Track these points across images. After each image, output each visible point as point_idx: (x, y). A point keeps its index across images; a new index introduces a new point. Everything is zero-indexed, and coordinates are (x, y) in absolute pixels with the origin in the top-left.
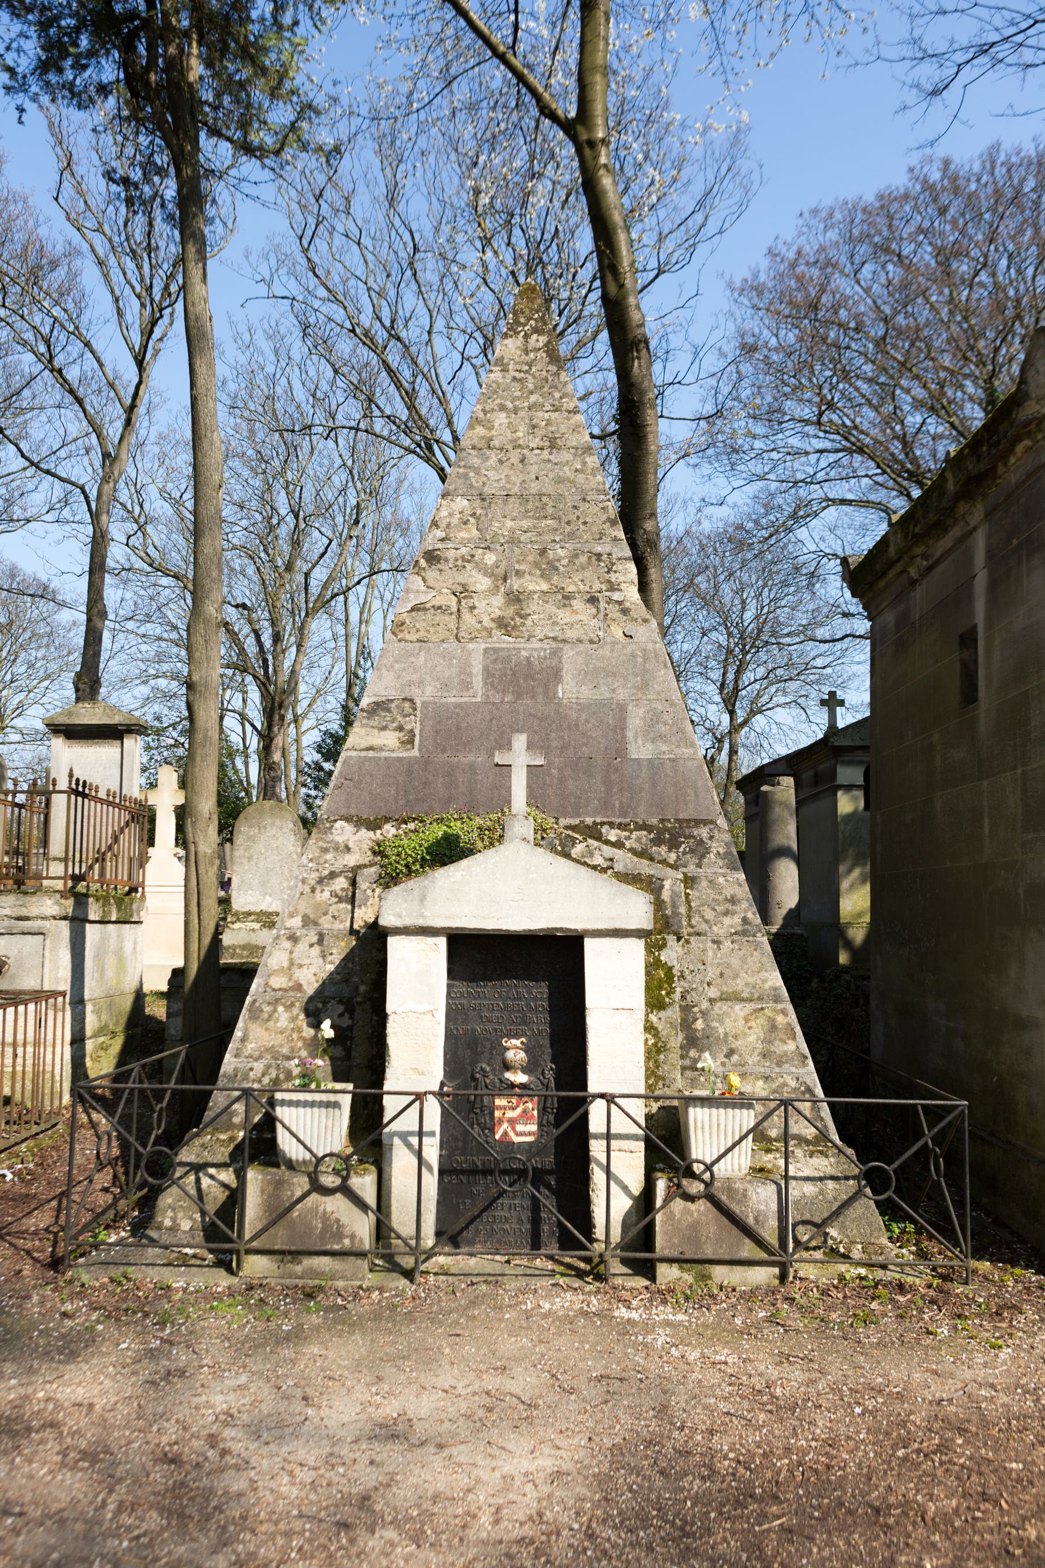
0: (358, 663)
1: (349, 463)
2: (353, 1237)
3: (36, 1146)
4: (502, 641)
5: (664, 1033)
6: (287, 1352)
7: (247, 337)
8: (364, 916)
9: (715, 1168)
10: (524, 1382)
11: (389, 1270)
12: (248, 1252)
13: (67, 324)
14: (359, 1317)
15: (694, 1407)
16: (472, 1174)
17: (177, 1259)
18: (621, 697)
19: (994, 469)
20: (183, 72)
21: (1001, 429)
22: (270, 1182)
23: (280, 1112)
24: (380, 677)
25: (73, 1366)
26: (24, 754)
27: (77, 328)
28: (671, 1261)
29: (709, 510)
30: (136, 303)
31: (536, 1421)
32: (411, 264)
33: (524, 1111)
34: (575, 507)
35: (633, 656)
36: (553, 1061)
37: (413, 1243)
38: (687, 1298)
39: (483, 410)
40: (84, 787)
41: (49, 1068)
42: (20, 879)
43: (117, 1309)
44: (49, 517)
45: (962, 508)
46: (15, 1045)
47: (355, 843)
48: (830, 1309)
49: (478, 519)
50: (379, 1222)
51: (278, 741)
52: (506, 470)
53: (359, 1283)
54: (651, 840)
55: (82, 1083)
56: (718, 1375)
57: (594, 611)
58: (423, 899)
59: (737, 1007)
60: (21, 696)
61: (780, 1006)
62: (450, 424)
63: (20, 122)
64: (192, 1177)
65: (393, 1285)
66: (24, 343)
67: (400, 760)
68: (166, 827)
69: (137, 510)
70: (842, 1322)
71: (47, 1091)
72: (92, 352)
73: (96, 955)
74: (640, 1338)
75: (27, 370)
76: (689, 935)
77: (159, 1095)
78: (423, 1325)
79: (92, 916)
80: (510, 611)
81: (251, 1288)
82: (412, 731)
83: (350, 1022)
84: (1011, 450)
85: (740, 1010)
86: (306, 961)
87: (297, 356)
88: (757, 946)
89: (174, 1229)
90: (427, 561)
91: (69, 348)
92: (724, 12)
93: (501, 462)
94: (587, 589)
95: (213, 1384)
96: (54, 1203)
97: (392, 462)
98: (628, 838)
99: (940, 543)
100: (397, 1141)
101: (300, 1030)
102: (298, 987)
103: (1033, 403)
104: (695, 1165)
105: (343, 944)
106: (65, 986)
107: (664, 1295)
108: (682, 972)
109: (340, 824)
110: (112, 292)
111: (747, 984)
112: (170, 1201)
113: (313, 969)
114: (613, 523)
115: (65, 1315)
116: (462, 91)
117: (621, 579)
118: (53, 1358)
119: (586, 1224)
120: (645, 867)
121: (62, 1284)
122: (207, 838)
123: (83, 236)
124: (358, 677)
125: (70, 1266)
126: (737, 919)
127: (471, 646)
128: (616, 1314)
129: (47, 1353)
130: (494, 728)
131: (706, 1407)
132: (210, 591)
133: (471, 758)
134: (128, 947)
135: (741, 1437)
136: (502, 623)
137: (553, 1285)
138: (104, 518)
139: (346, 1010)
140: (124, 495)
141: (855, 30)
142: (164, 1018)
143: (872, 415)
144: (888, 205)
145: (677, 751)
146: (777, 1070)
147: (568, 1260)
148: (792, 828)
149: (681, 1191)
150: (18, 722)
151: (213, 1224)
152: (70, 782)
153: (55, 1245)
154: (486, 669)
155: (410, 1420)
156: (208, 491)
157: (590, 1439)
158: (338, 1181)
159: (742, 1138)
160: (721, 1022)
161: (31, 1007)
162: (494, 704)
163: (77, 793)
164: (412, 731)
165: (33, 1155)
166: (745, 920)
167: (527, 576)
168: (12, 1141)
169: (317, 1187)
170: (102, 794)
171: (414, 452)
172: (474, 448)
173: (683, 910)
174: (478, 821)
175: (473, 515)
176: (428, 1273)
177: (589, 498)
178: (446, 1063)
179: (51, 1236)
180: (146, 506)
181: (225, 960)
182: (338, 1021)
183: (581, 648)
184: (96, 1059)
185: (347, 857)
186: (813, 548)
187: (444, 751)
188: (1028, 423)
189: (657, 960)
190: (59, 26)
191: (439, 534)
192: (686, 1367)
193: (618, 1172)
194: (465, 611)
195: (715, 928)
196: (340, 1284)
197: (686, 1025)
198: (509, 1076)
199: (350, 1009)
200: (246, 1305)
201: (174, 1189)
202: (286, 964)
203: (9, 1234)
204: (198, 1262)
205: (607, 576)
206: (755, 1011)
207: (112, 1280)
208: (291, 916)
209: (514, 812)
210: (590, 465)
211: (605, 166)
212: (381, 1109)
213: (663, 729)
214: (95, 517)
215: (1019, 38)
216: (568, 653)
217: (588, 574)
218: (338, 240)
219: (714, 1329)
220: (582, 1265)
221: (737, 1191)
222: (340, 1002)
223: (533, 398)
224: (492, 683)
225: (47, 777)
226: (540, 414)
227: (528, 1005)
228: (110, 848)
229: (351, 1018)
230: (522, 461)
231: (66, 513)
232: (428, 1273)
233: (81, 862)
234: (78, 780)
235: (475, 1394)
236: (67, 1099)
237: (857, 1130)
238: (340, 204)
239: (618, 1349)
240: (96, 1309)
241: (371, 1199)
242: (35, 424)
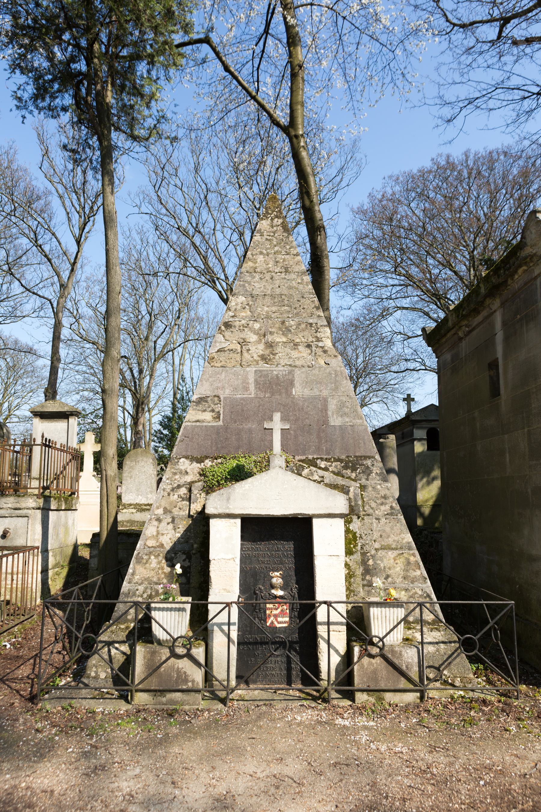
0: (179, 383)
2: (193, 681)
3: (23, 628)
4: (266, 367)
5: (353, 567)
6: (161, 752)
7: (128, 233)
9: (385, 640)
10: (293, 768)
11: (213, 699)
12: (137, 691)
13: (44, 225)
14: (199, 728)
15: (391, 783)
16: (254, 644)
17: (98, 695)
18: (325, 394)
19: (506, 281)
20: (104, 97)
21: (511, 262)
23: (154, 614)
25: (42, 765)
26: (19, 427)
27: (49, 227)
28: (362, 691)
29: (343, 312)
30: (77, 216)
31: (304, 794)
32: (206, 197)
33: (282, 610)
34: (298, 301)
35: (330, 374)
36: (297, 583)
37: (225, 683)
38: (373, 712)
39: (252, 254)
40: (49, 442)
41: (30, 586)
42: (18, 489)
43: (66, 726)
44: (35, 314)
45: (488, 301)
46: (12, 574)
47: (189, 470)
48: (450, 716)
49: (250, 306)
50: (206, 673)
51: (141, 420)
52: (263, 283)
53: (197, 707)
54: (343, 467)
55: (48, 600)
56: (399, 761)
57: (309, 351)
58: (228, 499)
59: (390, 553)
60: (19, 400)
61: (411, 552)
62: (224, 271)
63: (23, 122)
64: (106, 649)
65: (215, 708)
67: (213, 427)
68: (89, 462)
69: (75, 312)
70: (458, 724)
71: (29, 597)
72: (56, 238)
73: (54, 527)
74: (353, 737)
75: (25, 247)
76: (364, 515)
77: (88, 604)
78: (234, 732)
79: (52, 508)
80: (267, 352)
81: (139, 711)
82: (219, 412)
83: (189, 564)
84: (516, 272)
85: (391, 554)
86: (166, 532)
87: (151, 242)
88: (399, 521)
89: (96, 677)
90: (225, 327)
91: (45, 236)
92: (355, 81)
93: (261, 279)
94: (306, 340)
95: (121, 775)
96: (32, 661)
97: (195, 290)
98: (331, 466)
99: (476, 319)
100: (215, 628)
101: (163, 568)
102: (162, 546)
103: (529, 248)
104: (374, 639)
105: (185, 522)
106: (38, 544)
107: (361, 710)
108: (361, 535)
109: (182, 460)
110: (66, 210)
111: (394, 541)
112: (94, 662)
113: (169, 536)
114: (318, 308)
115: (37, 730)
116: (231, 120)
117: (323, 336)
118: (31, 759)
119: (316, 671)
120: (340, 481)
121: (35, 711)
122: (111, 468)
124: (179, 390)
125: (40, 700)
126: (388, 507)
127: (248, 369)
128: (337, 722)
129: (27, 756)
130: (261, 410)
131: (398, 782)
132: (114, 344)
133: (249, 425)
134: (70, 522)
135: (421, 802)
136: (263, 358)
137: (301, 705)
138: (60, 314)
139: (187, 557)
140: (69, 305)
141: (414, 91)
142: (88, 557)
143: (417, 269)
144: (423, 174)
145: (354, 421)
146: (412, 585)
147: (307, 691)
148: (395, 459)
149: (367, 653)
150: (17, 413)
151: (117, 675)
152: (42, 440)
153: (32, 687)
154: (256, 381)
155: (233, 796)
156: (114, 295)
157: (337, 806)
158: (185, 651)
159: (398, 624)
161: (21, 555)
162: (260, 398)
163: (46, 445)
164: (219, 412)
165: (21, 633)
166: (392, 507)
167: (275, 334)
168: (10, 626)
169: (174, 655)
170: (58, 446)
171: (207, 284)
172: (247, 272)
173: (360, 502)
174: (254, 458)
175: (248, 304)
176: (234, 700)
177: (305, 296)
178: (241, 585)
179: (30, 681)
180: (80, 311)
181: (120, 528)
183: (304, 369)
184: (54, 580)
185: (186, 477)
186: (390, 329)
187: (235, 422)
188: (526, 258)
190: (44, 80)
191: (231, 314)
192: (381, 756)
194: (244, 352)
195: (377, 512)
196: (187, 707)
197: (364, 562)
198: (274, 591)
199: (189, 557)
200: (137, 722)
201: (96, 656)
202: (155, 533)
203: (7, 680)
204: (110, 696)
205: (315, 334)
206: (399, 554)
208: (158, 508)
209: (275, 452)
210: (305, 280)
211: (303, 146)
212: (207, 611)
213: (346, 410)
214: (56, 314)
215: (489, 95)
216: (297, 372)
217: (306, 333)
218: (172, 188)
219: (391, 731)
220: (315, 693)
221: (396, 652)
222: (184, 553)
223: (276, 249)
224: (259, 388)
225: (31, 439)
226: (280, 256)
227: (283, 554)
228: (62, 472)
229: (189, 562)
230: (272, 278)
231: (42, 313)
232: (234, 700)
233: (47, 480)
234: (46, 439)
235: (268, 777)
236: (39, 601)
237: (453, 617)
238: (172, 171)
239: (341, 744)
240: (55, 726)
241: (202, 660)
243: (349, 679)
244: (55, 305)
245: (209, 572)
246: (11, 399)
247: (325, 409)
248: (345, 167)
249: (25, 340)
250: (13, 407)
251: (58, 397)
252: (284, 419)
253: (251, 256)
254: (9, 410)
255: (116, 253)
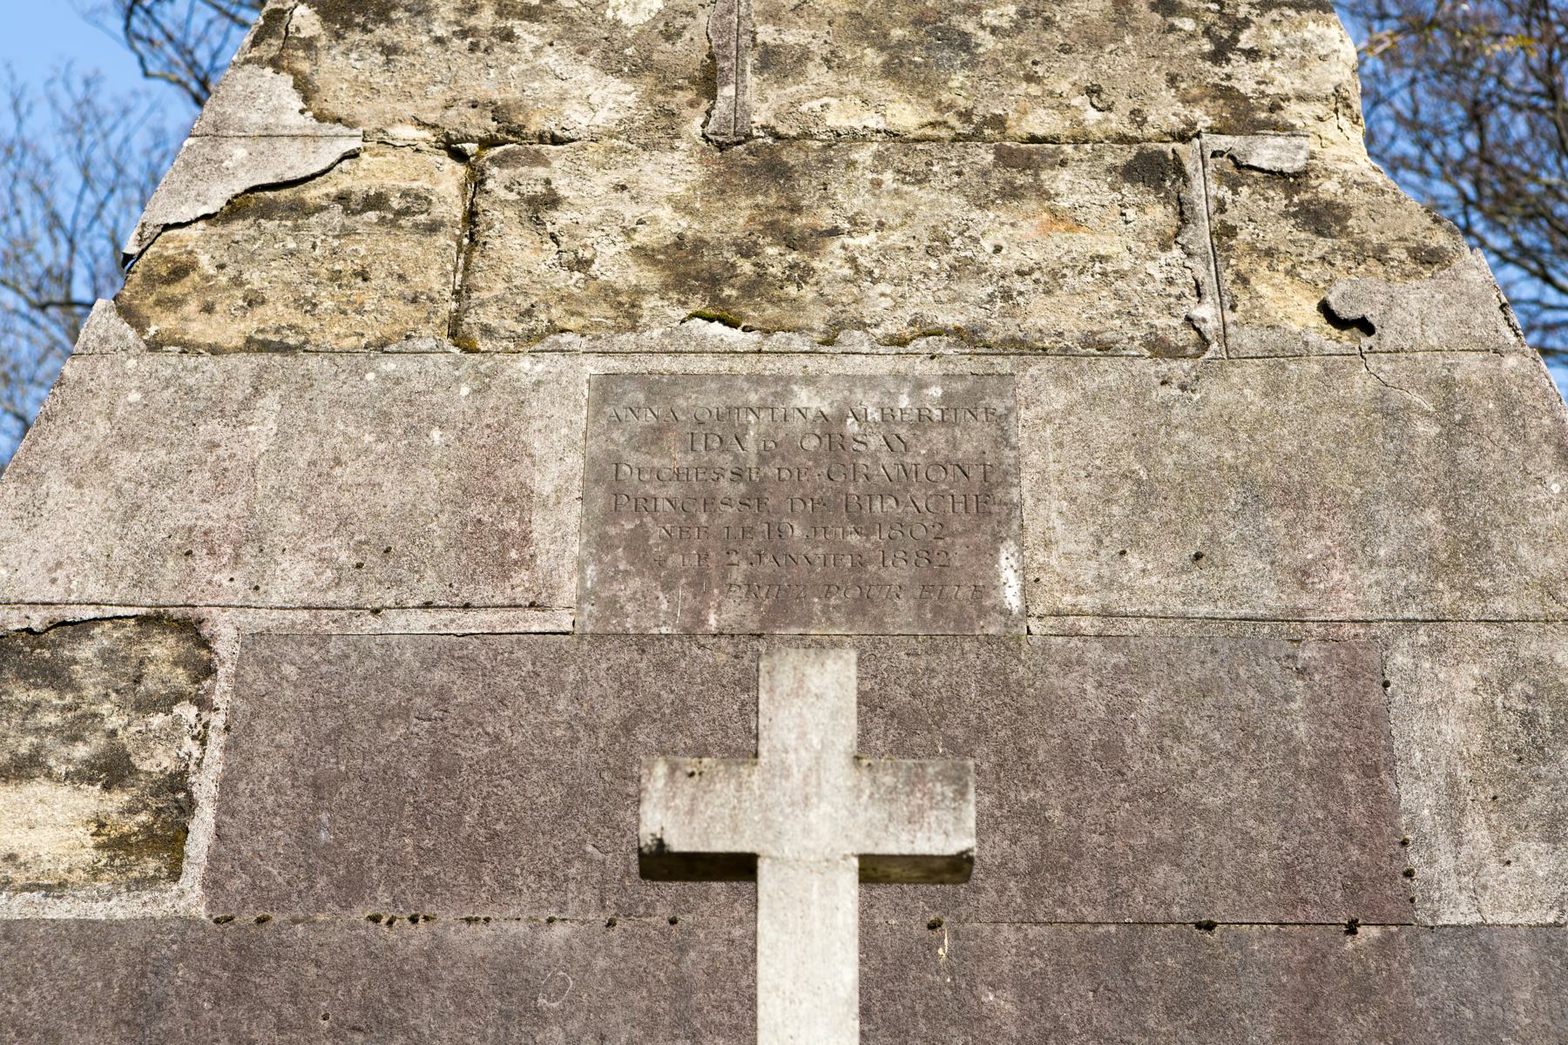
67: (88, 935)
127: (526, 366)
136: (689, 270)
183: (1109, 373)
187: (351, 889)
216: (1042, 397)
247: (1361, 751)
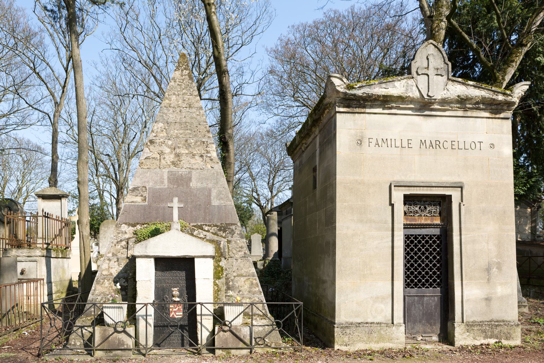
1: (142, 107)
2: (127, 345)
4: (175, 169)
7: (106, 62)
8: (130, 253)
9: (232, 323)
12: (96, 350)
19: (320, 118)
22: (102, 330)
24: (135, 180)
30: (64, 50)
35: (214, 174)
38: (223, 358)
44: (39, 123)
58: (146, 247)
59: (242, 278)
60: (34, 185)
64: (80, 330)
66: (26, 63)
67: (141, 205)
73: (55, 268)
80: (176, 159)
85: (243, 279)
89: (75, 345)
93: (173, 111)
100: (140, 318)
101: (112, 287)
102: (111, 274)
109: (123, 225)
113: (116, 269)
119: (196, 340)
120: (216, 238)
123: (45, 25)
126: (243, 253)
127: (164, 170)
134: (66, 266)
136: (173, 163)
138: (57, 124)
140: (65, 116)
142: (77, 287)
147: (191, 350)
151: (87, 343)
154: (168, 177)
158: (122, 329)
160: (237, 282)
163: (45, 217)
166: (245, 253)
169: (116, 331)
173: (227, 250)
174: (166, 224)
175: (165, 128)
182: (123, 284)
183: (198, 171)
187: (155, 203)
188: (327, 105)
189: (219, 266)
191: (154, 134)
193: (205, 325)
194: (162, 159)
197: (227, 283)
198: (174, 299)
199: (127, 280)
201: (75, 334)
202: (107, 267)
207: (56, 359)
208: (109, 253)
210: (201, 113)
213: (222, 196)
214: (53, 124)
216: (194, 172)
217: (200, 148)
220: (195, 351)
222: (124, 278)
223: (184, 91)
226: (186, 96)
238: (135, 17)
241: (133, 334)
242: (32, 91)
243: (213, 342)
244: (52, 117)
245: (136, 288)
246: (28, 184)
247: (209, 195)
248: (260, 17)
249: (34, 141)
250: (30, 190)
251: (59, 183)
252: (180, 201)
253: (167, 96)
254: (27, 192)
255: (82, 90)
